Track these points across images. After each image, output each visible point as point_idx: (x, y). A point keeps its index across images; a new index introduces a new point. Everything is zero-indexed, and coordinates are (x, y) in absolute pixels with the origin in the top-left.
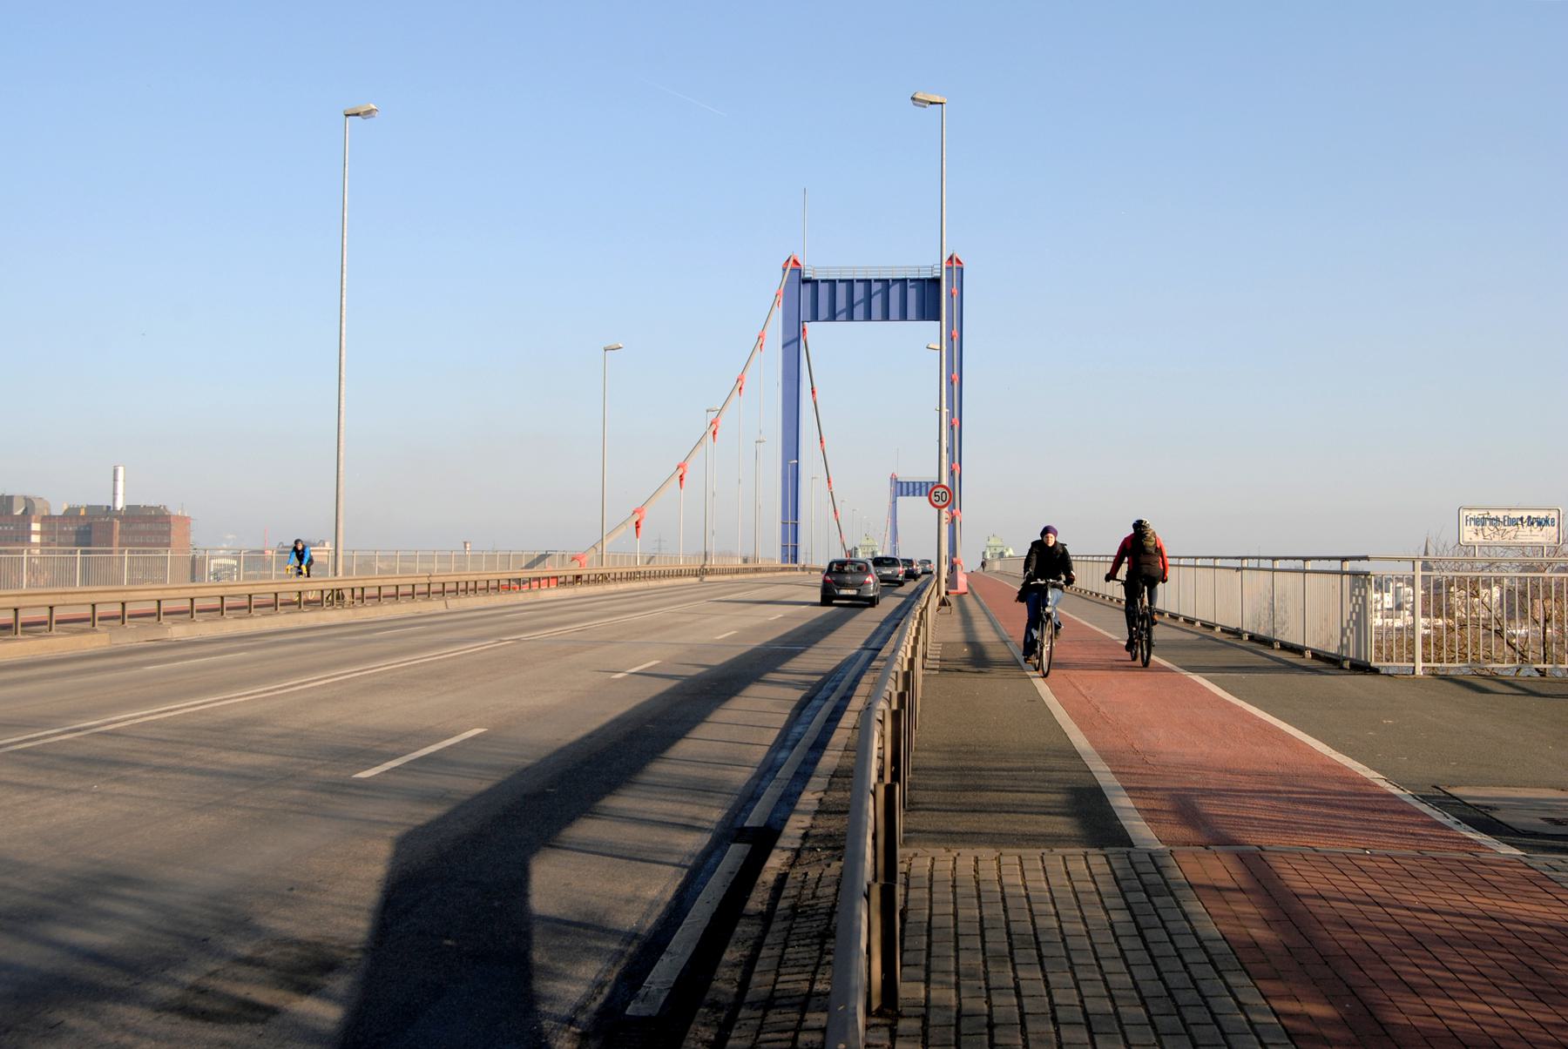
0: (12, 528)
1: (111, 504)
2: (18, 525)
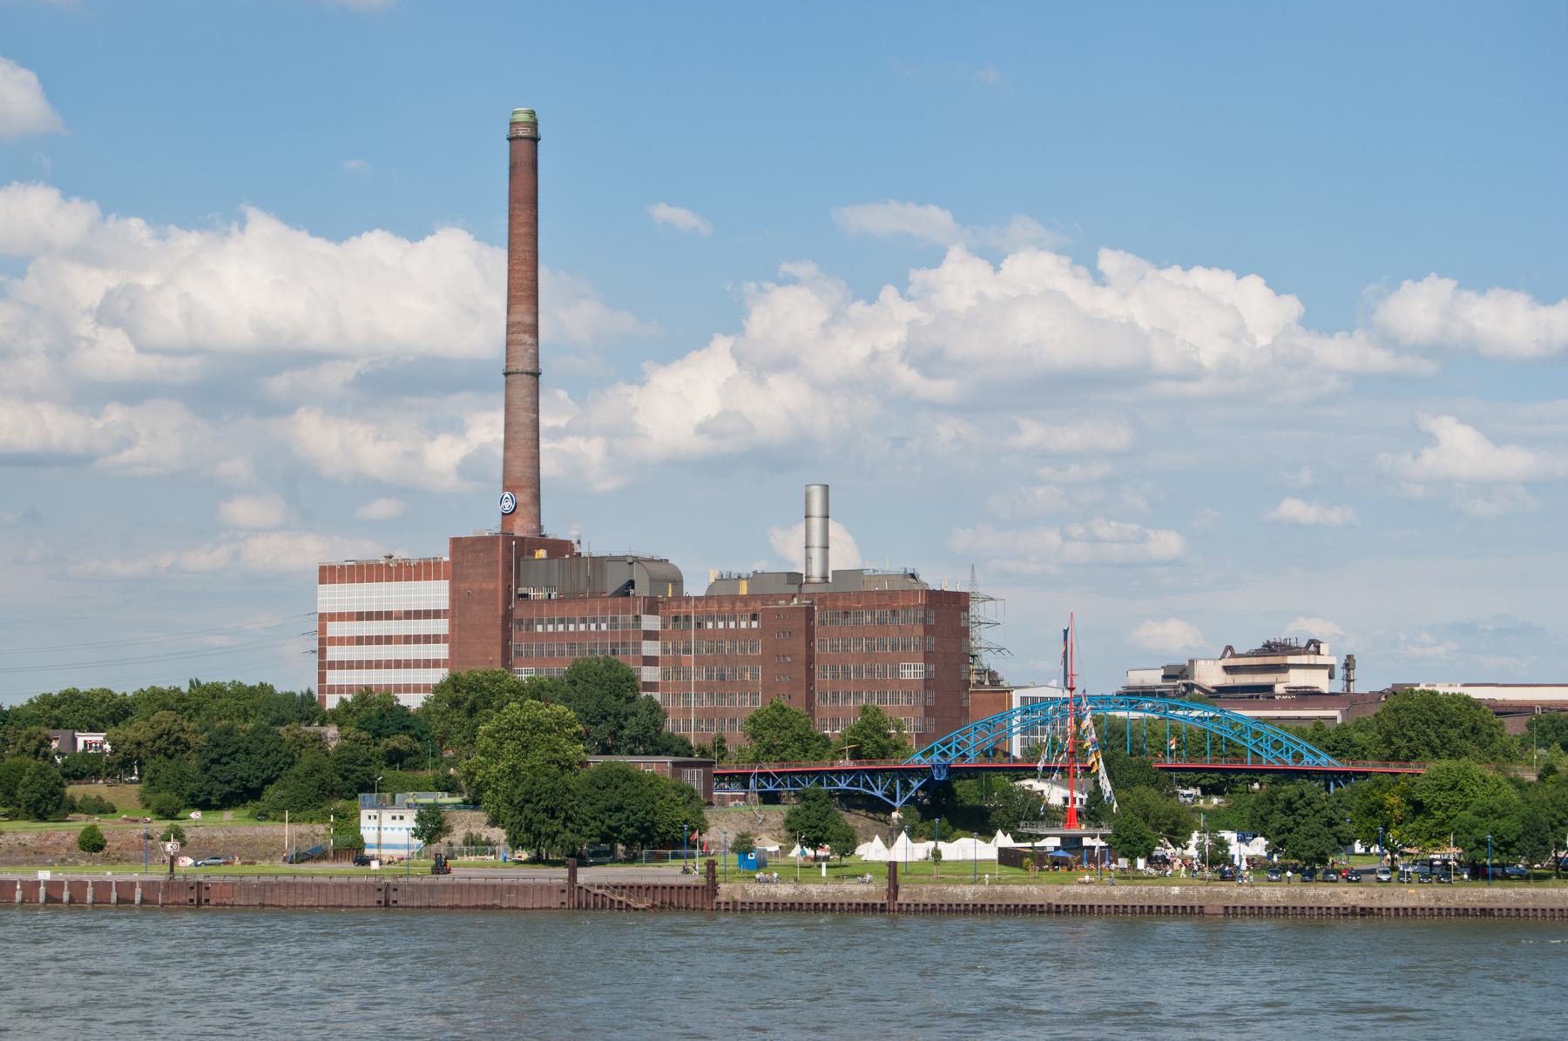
0: (604, 627)
1: (802, 570)
2: (614, 620)
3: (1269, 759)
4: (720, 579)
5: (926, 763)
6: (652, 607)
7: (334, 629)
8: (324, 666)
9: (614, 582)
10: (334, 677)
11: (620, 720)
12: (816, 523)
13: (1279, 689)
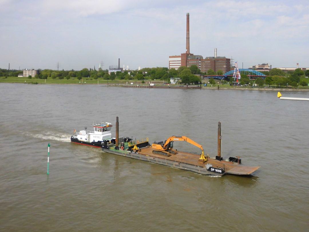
1: (214, 56)
3: (259, 75)
4: (206, 57)
5: (225, 75)
6: (200, 60)
7: (170, 62)
8: (170, 66)
9: (196, 58)
10: (170, 67)
11: (196, 71)
12: (216, 52)
13: (264, 68)
